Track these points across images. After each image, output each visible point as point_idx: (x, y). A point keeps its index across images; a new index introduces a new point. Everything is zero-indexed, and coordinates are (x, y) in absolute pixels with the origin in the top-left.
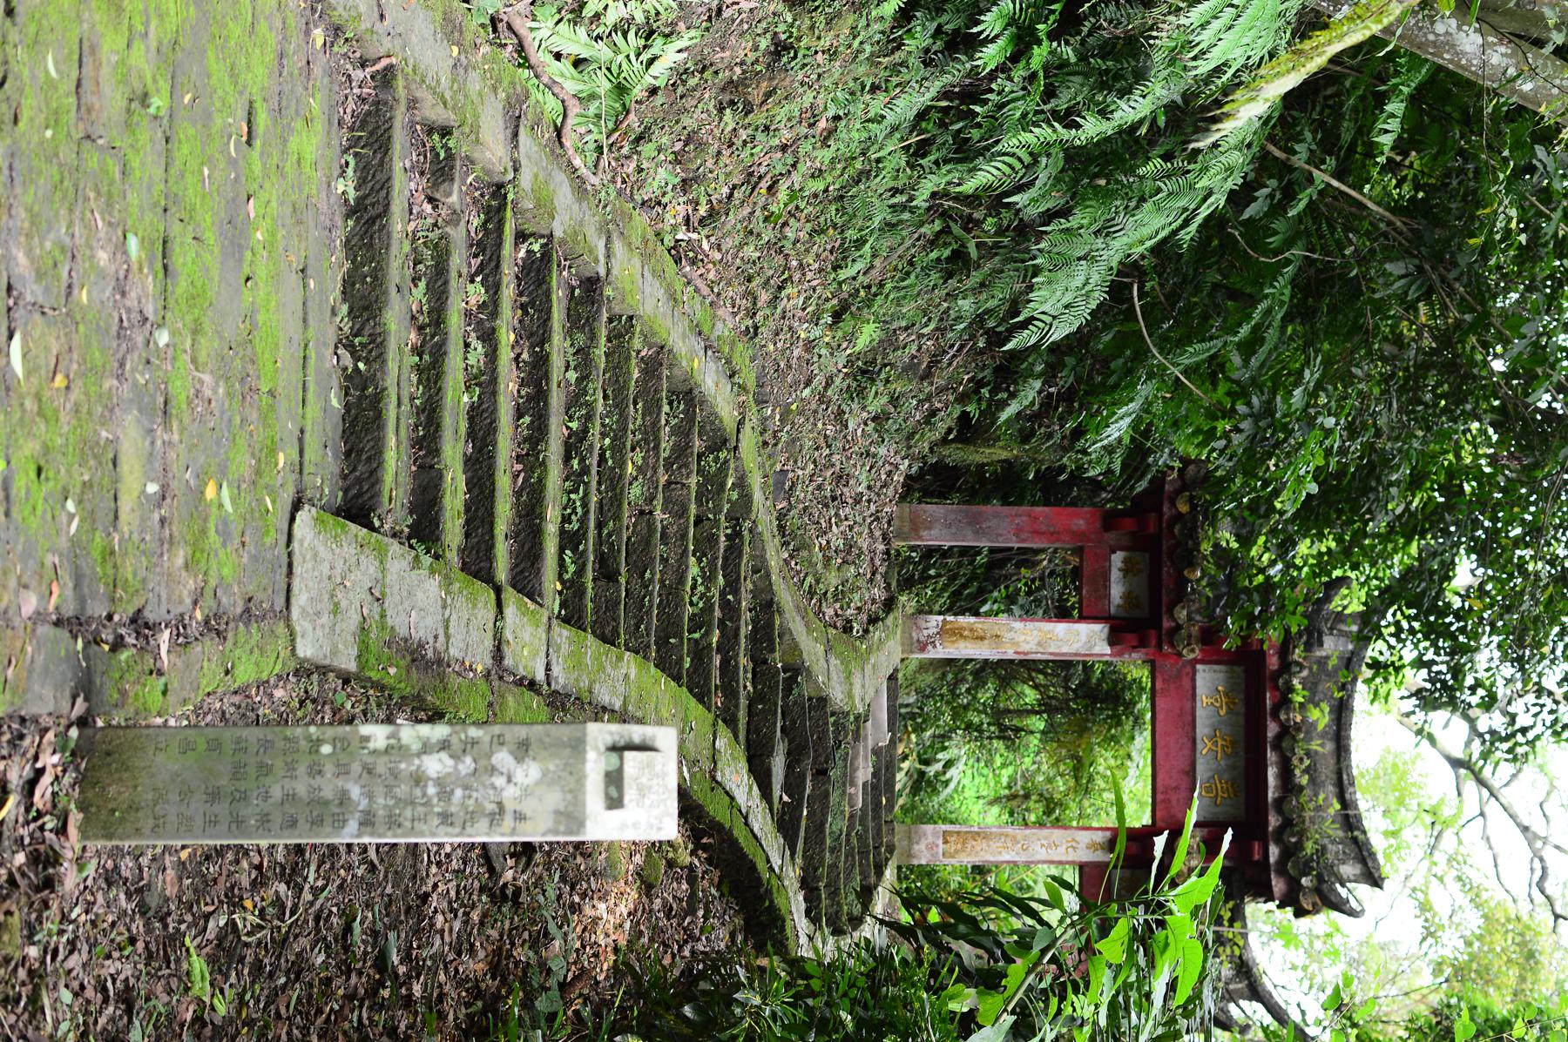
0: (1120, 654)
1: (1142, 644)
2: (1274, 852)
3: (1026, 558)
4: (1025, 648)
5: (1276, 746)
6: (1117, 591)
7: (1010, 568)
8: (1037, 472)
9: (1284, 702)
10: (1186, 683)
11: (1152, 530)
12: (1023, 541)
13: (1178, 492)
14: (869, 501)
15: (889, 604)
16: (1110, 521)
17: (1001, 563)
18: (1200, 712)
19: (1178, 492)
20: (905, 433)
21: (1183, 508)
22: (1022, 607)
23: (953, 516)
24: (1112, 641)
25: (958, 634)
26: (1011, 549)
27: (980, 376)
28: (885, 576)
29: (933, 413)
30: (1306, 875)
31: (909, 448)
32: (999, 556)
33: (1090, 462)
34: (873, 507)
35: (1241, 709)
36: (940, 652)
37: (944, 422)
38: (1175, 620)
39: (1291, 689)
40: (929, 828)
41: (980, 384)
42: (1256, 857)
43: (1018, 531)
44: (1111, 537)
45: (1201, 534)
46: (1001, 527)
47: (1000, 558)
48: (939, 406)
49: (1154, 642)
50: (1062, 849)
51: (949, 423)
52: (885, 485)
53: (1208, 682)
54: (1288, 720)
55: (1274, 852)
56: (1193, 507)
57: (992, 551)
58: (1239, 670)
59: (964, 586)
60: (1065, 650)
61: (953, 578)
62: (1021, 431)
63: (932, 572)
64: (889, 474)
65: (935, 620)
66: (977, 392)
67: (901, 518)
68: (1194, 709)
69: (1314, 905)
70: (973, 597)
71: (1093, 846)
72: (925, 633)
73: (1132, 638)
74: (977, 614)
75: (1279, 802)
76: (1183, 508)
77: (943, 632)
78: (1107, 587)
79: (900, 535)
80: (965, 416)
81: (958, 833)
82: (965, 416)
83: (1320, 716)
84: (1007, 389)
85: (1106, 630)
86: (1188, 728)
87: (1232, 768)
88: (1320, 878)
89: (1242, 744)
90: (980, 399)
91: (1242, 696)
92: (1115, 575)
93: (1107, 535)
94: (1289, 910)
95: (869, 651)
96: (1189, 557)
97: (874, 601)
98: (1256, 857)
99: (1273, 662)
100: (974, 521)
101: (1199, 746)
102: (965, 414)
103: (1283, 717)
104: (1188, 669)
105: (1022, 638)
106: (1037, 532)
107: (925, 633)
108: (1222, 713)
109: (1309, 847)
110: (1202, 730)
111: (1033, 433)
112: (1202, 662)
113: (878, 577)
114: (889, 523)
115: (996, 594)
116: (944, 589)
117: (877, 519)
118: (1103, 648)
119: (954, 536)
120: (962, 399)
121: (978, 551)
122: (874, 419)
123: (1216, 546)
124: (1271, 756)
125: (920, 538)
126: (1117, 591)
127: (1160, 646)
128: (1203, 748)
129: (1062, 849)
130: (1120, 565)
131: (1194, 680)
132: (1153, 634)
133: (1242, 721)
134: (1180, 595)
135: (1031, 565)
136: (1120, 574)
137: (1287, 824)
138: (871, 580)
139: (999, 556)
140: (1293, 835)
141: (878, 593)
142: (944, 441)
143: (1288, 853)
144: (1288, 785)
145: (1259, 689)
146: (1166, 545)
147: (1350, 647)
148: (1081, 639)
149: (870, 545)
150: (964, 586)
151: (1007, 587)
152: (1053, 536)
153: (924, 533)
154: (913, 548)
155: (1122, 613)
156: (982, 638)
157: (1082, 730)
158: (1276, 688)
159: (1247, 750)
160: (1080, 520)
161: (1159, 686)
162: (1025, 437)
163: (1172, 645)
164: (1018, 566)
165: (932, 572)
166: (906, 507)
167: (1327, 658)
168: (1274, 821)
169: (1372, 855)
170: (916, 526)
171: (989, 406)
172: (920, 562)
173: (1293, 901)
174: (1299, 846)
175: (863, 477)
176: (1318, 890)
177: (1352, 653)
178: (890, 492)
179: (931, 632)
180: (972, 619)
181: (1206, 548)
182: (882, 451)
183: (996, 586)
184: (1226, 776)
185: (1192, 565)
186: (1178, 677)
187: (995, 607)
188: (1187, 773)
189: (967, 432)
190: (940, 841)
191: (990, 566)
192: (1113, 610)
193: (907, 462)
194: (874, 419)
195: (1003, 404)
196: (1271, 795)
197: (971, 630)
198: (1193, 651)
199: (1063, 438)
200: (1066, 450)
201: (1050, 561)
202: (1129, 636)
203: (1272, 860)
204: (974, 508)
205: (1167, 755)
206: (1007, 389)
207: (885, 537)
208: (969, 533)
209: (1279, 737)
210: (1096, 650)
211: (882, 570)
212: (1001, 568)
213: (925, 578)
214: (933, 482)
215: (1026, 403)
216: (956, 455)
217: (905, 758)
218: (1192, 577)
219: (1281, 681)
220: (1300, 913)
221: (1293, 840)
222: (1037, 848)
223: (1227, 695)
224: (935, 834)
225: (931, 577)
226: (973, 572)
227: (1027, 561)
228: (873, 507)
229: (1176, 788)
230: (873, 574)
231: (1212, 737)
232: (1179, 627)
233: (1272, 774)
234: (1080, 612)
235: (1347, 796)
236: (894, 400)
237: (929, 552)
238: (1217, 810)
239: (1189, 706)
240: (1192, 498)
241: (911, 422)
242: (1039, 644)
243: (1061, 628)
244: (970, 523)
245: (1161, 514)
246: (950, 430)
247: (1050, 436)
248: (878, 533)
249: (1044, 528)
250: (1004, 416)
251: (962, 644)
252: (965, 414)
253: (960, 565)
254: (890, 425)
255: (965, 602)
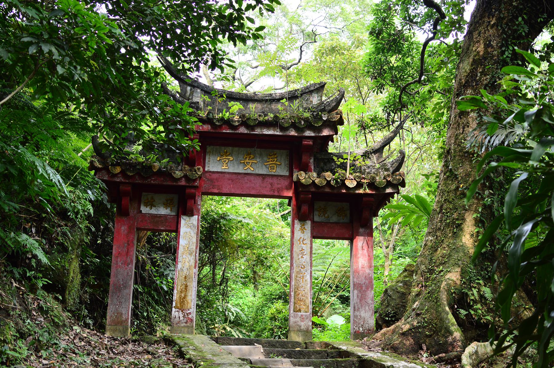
0: (198, 211)
1: (193, 197)
2: (308, 133)
3: (140, 266)
4: (192, 262)
5: (252, 128)
6: (163, 211)
7: (145, 275)
8: (96, 257)
9: (228, 123)
10: (215, 176)
11: (129, 188)
12: (132, 261)
13: (108, 172)
14: (98, 354)
15: (169, 342)
16: (123, 212)
17: (143, 278)
18: (231, 170)
19: (108, 172)
20: (52, 329)
21: (118, 170)
22: (165, 270)
23: (115, 301)
24: (190, 213)
25: (183, 300)
26: (135, 273)
27: (17, 276)
28: (150, 344)
29: (40, 309)
30: (321, 117)
31: (64, 325)
32: (139, 279)
33: (84, 211)
34: (103, 352)
35: (229, 149)
36: (193, 310)
37: (50, 302)
38: (181, 178)
39: (222, 119)
40: (292, 320)
41: (24, 276)
42: (311, 143)
43: (126, 264)
44: (132, 212)
45: (134, 161)
46: (123, 273)
47: (140, 279)
48: (36, 304)
49: (193, 191)
50: (304, 247)
51: (50, 298)
52: (89, 343)
53: (215, 165)
54: (238, 121)
55: (308, 133)
56: (118, 164)
57: (136, 283)
58: (209, 149)
59: (153, 298)
60: (194, 240)
61: (149, 303)
62: (59, 252)
63: (145, 314)
64: (81, 339)
65: (175, 313)
66: (29, 279)
67: (114, 331)
68: (229, 173)
69: (337, 114)
70: (159, 293)
71: (303, 230)
72: (182, 318)
73: (190, 203)
74: (170, 292)
75: (283, 129)
76: (118, 170)
77: (181, 309)
78: (160, 216)
79: (125, 332)
80: (46, 288)
81: (295, 303)
82: (46, 288)
83: (236, 107)
84: (30, 259)
85: (184, 217)
86: (239, 177)
87: (261, 155)
88: (323, 110)
89: (249, 149)
90: (35, 278)
91: (223, 148)
92: (154, 211)
93: (131, 214)
94: (339, 127)
95: (204, 359)
96: (147, 168)
97: (167, 353)
98: (311, 143)
99: (207, 128)
100: (119, 289)
101: (249, 172)
102: (45, 287)
103: (237, 124)
104: (207, 175)
105: (187, 264)
106: (127, 253)
107: (182, 318)
108: (232, 159)
109: (307, 115)
110: (240, 170)
111: (62, 244)
112: (204, 167)
113: (150, 349)
114: (115, 340)
115: (158, 282)
116: (153, 307)
117: (111, 348)
118: (195, 219)
119: (127, 300)
120: (33, 289)
121: (136, 290)
122: (37, 350)
123: (141, 153)
124: (258, 131)
125: (127, 320)
126: (163, 211)
127: (196, 187)
128: (250, 170)
129: (304, 247)
130: (148, 209)
131: (214, 172)
132: (188, 191)
133: (236, 149)
134: (166, 174)
135: (144, 263)
136: (153, 208)
137: (294, 126)
138: (153, 354)
139: (139, 279)
140: (300, 122)
141: (161, 349)
142: (63, 302)
143: (309, 126)
144: (274, 123)
145: (222, 137)
146: (138, 181)
147: (199, 91)
148: (189, 232)
149: (129, 354)
150: (153, 298)
151: (155, 276)
152: (130, 244)
153: (124, 317)
154: (132, 323)
155: (175, 209)
156: (186, 286)
157: (226, 244)
158: (220, 127)
159: (251, 146)
160: (121, 229)
161: (216, 191)
162: (64, 249)
163: (195, 180)
164: (144, 270)
165: (145, 314)
166: (108, 327)
167: (204, 101)
168: (293, 133)
169: (307, 88)
170: (119, 322)
171: (40, 272)
172: (140, 320)
173: (335, 124)
174: (306, 120)
175: (80, 359)
176: (330, 111)
177: (202, 90)
178: (94, 339)
179: (181, 315)
180: (175, 292)
181: (141, 159)
182: (63, 344)
183: (154, 282)
184: (265, 159)
185: (150, 167)
186: (211, 180)
187: (164, 282)
188: (264, 179)
189: (57, 287)
190: (299, 314)
191: (144, 284)
192: (174, 214)
193: (75, 328)
194: (37, 350)
195: (39, 262)
196: (278, 133)
197: (181, 292)
198: (199, 169)
199: (66, 225)
200: (75, 225)
201: (143, 255)
202: (189, 204)
203: (313, 134)
204: (111, 288)
205: (253, 188)
206: (30, 259)
207: (124, 343)
208: (125, 291)
209: (247, 126)
210: (195, 223)
211: (145, 346)
212: (145, 279)
213: (148, 318)
214: (94, 311)
215: (37, 245)
216: (72, 297)
217: (224, 329)
218: (157, 168)
219: (217, 123)
220: (341, 122)
221: (303, 123)
222: (303, 260)
223: (222, 156)
224: (295, 317)
225: (147, 315)
226: (146, 293)
227: (142, 266)
228: (103, 352)
229: (271, 184)
230: (148, 352)
231: (245, 165)
232: (185, 176)
233: (266, 132)
234: (171, 231)
235: (278, 97)
236: (22, 336)
237: (135, 315)
238: (283, 164)
239: (227, 176)
240: (113, 165)
241: (45, 324)
242: (191, 254)
243: (183, 242)
244: (120, 291)
245: (121, 183)
246: (56, 299)
247: (64, 234)
248: (121, 348)
249: (125, 249)
250: (44, 260)
251: (189, 298)
252: (45, 287)
253: (142, 300)
254: (44, 338)
255: (164, 299)
